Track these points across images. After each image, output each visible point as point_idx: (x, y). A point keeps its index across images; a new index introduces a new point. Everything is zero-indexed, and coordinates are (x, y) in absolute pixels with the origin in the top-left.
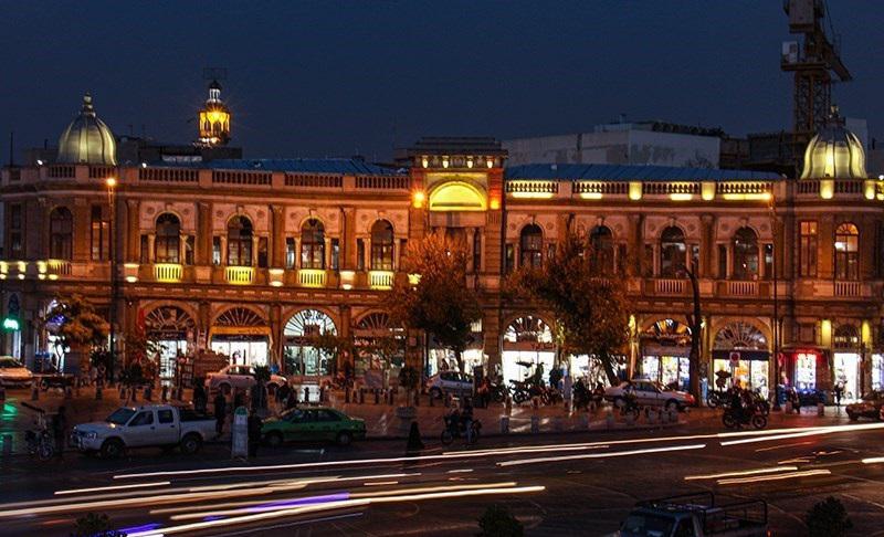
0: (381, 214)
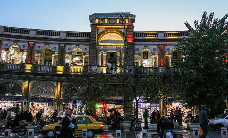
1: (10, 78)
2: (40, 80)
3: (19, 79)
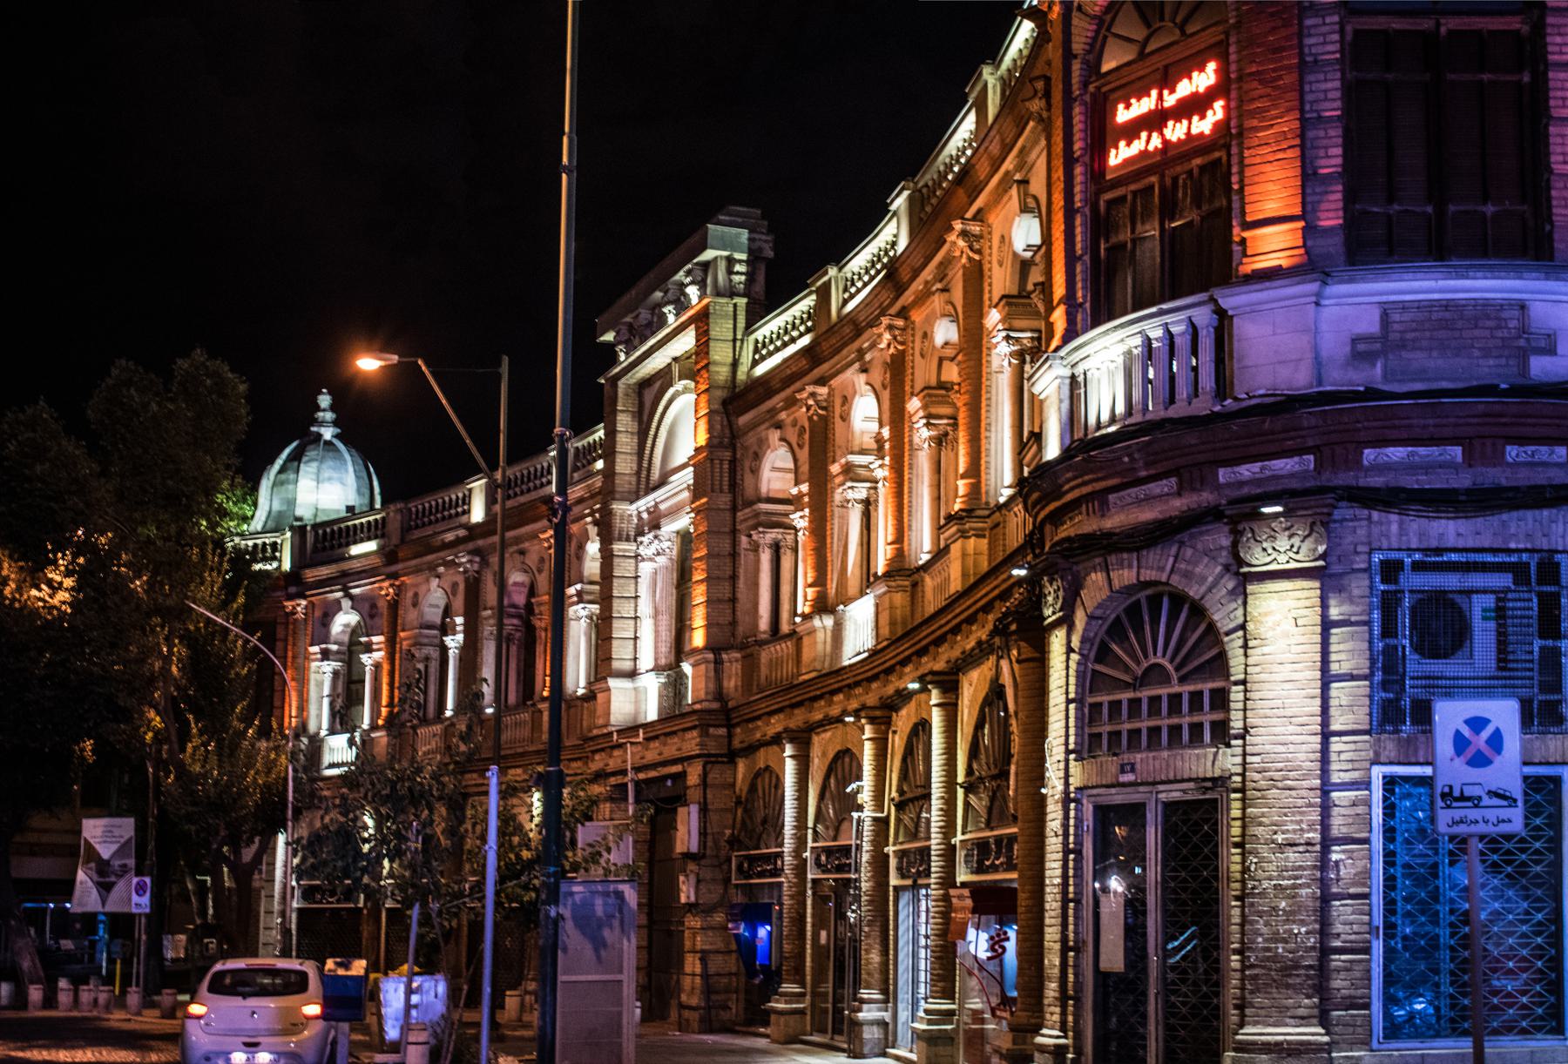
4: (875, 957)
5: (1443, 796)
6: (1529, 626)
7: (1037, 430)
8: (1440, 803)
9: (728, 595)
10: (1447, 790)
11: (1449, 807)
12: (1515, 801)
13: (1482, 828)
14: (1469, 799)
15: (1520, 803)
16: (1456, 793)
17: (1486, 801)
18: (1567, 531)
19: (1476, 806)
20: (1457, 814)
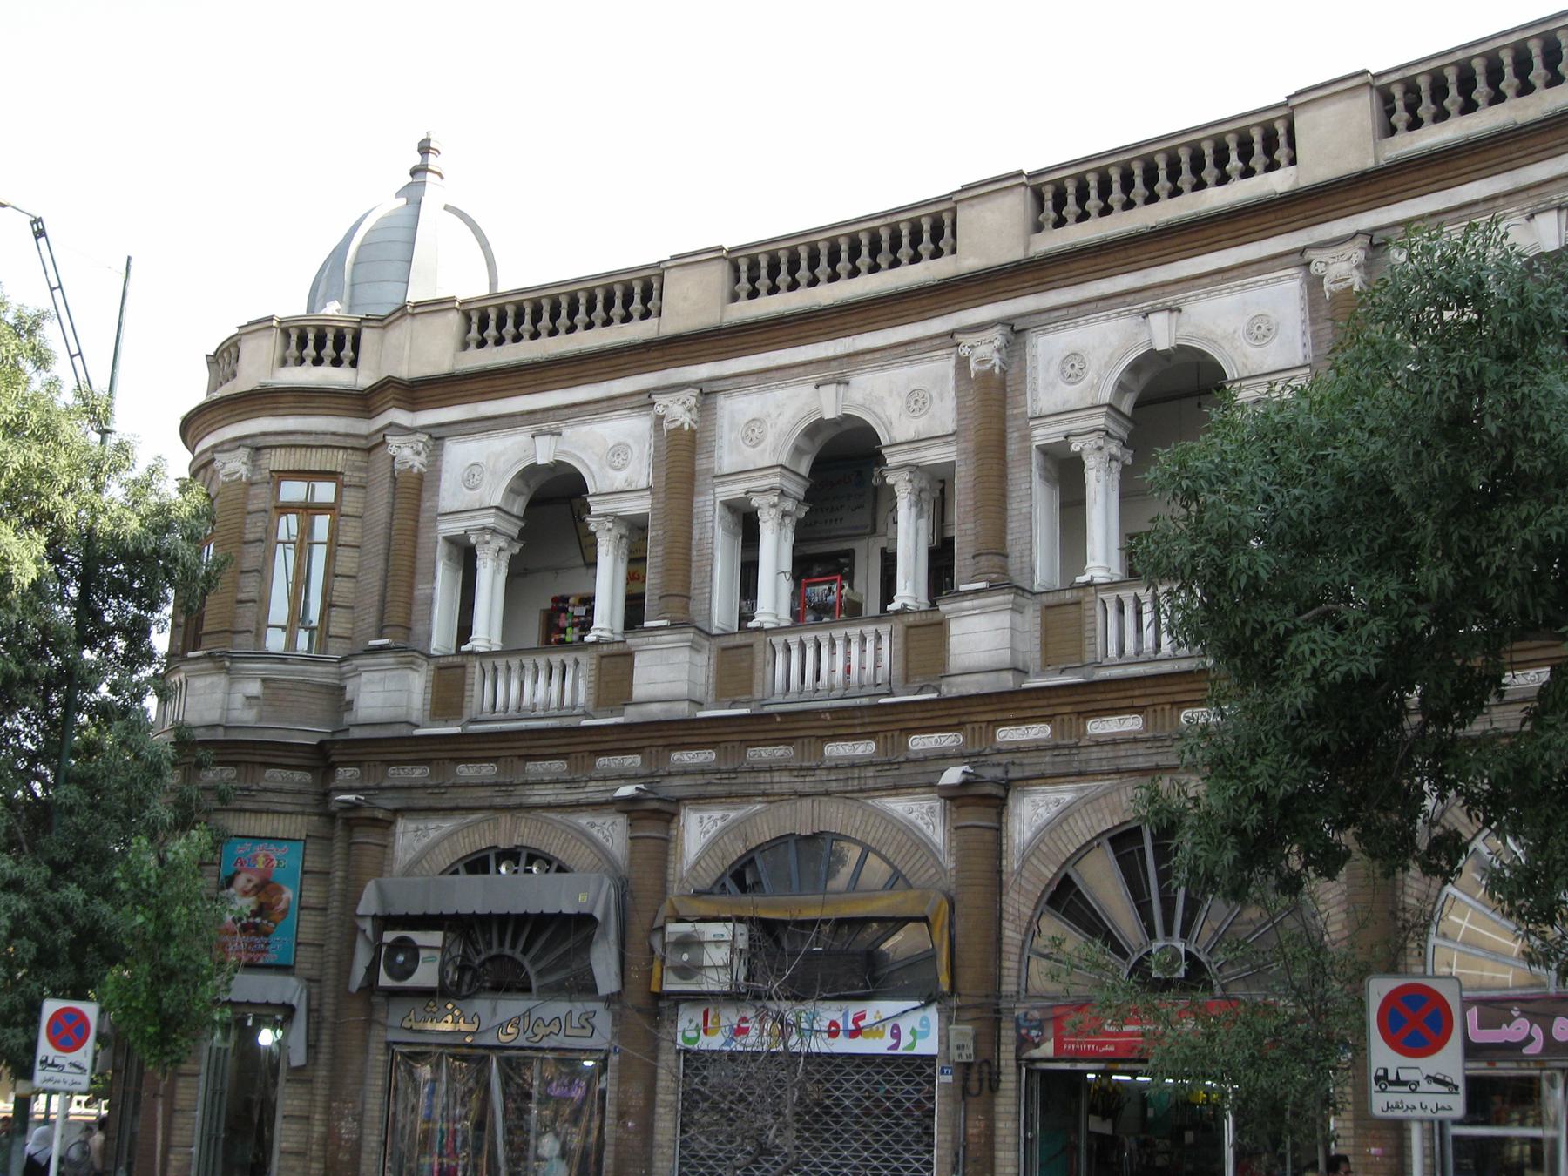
0: (1159, 321)
1: (807, 788)
2: (1118, 771)
3: (896, 789)
4: (655, 707)
5: (1378, 1079)
6: (1138, 603)
7: (42, 240)
8: (1375, 1087)
9: (334, 612)
10: (1381, 1073)
11: (1383, 1091)
12: (1456, 1087)
13: (1419, 1113)
14: (1405, 1083)
15: (1462, 1089)
16: (1392, 1077)
17: (1424, 1086)
18: (460, 1174)
19: (1413, 1091)
20: (1392, 1098)
